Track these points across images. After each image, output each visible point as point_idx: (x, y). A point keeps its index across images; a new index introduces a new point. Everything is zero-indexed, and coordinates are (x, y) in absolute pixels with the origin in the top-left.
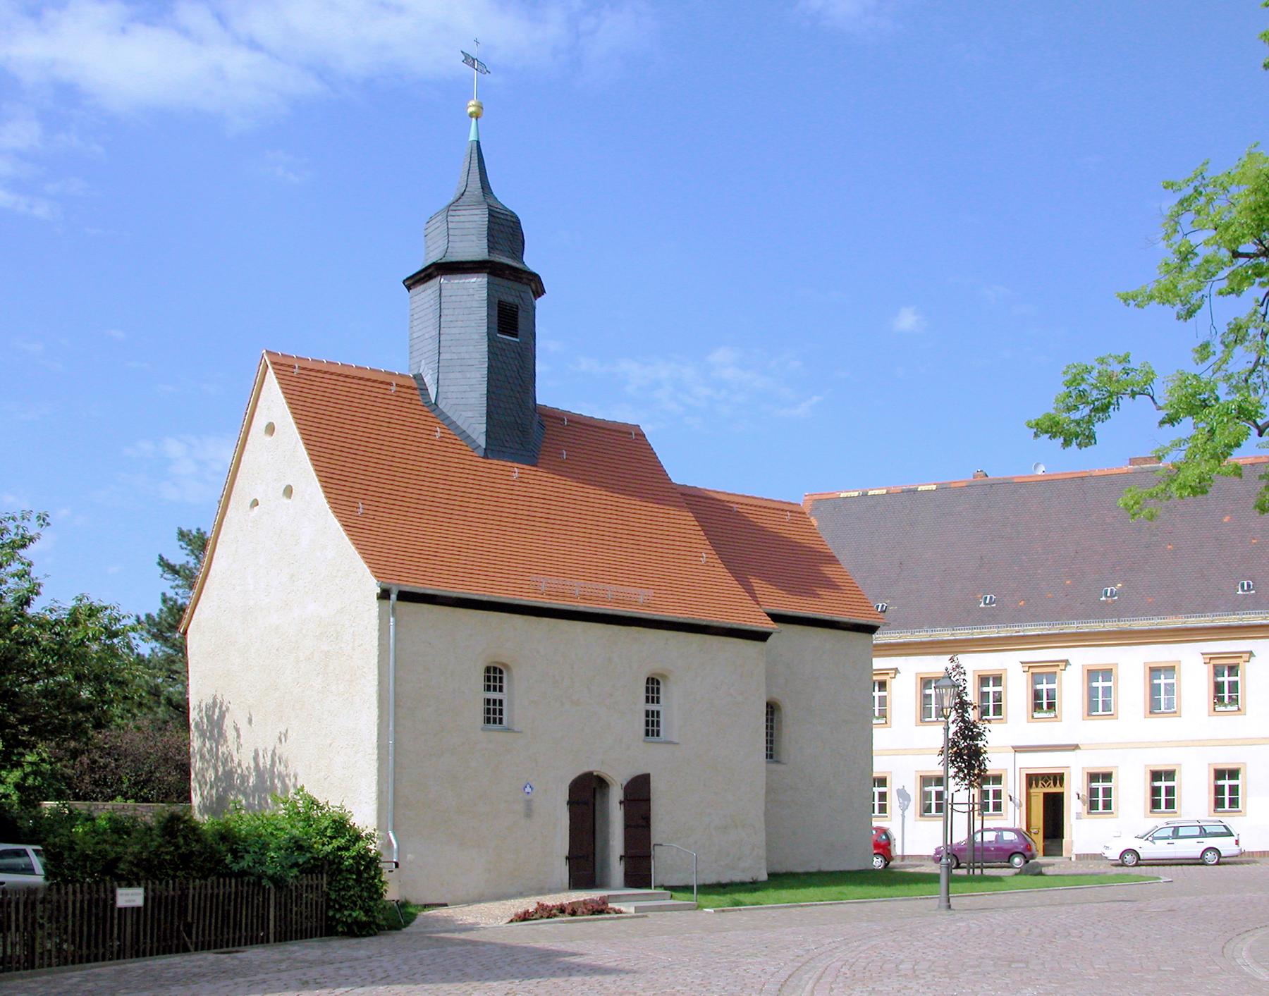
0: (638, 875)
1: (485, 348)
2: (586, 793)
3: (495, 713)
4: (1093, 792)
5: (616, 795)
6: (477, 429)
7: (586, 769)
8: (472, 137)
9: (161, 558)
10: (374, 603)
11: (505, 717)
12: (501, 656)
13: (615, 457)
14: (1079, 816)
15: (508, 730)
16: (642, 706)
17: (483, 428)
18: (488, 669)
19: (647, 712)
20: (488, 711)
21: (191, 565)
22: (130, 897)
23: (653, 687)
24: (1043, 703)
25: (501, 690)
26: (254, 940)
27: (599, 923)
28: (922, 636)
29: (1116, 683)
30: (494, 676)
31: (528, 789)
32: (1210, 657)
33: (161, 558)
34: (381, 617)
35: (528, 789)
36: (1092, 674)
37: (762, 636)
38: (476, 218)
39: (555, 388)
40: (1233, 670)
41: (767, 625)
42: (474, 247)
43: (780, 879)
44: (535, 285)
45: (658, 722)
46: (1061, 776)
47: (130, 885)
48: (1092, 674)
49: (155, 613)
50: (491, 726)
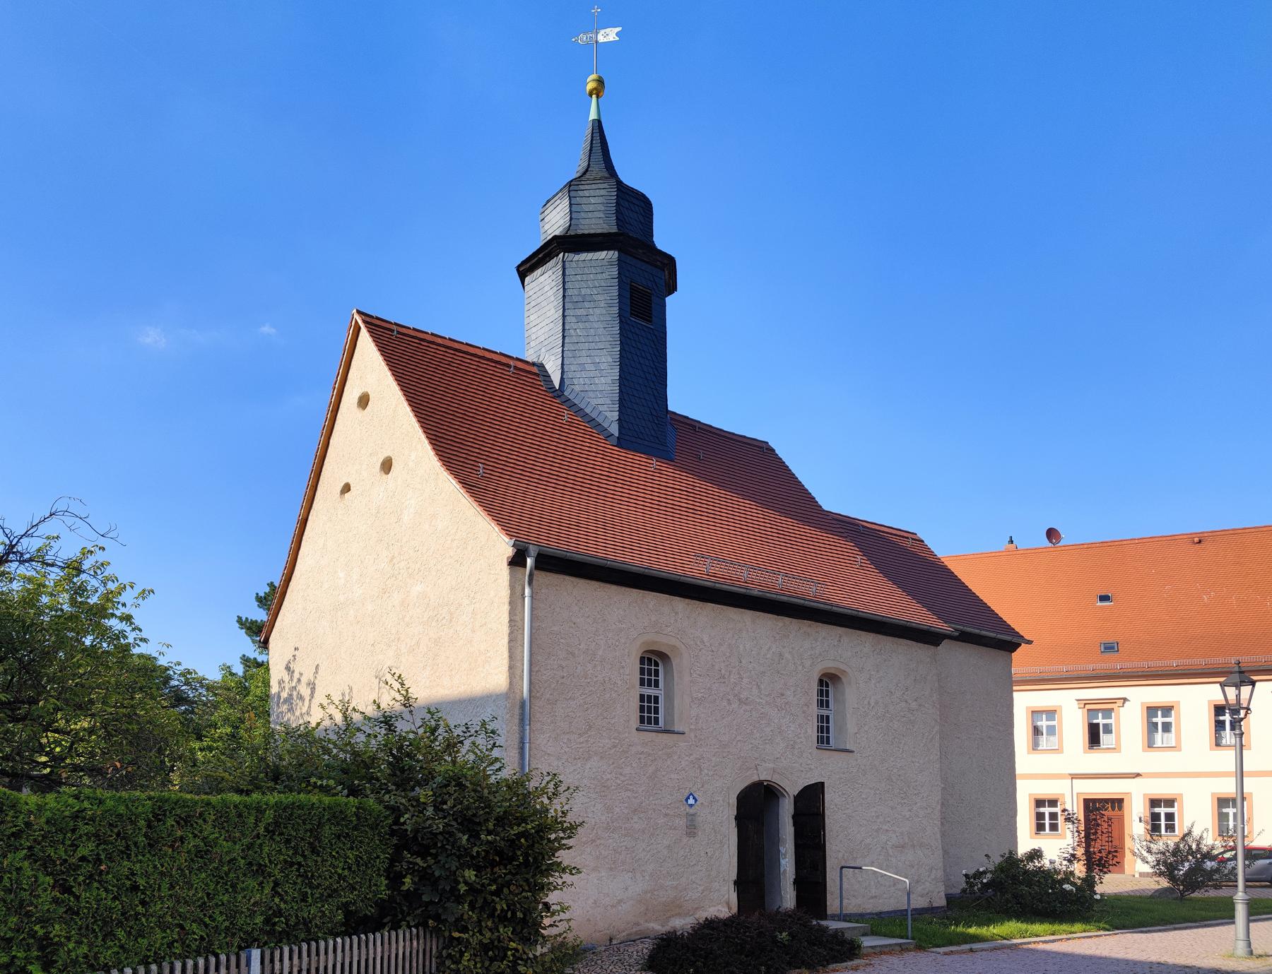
1: (616, 330)
2: (756, 804)
3: (649, 712)
4: (1155, 817)
5: (786, 810)
6: (610, 417)
7: (755, 778)
8: (593, 115)
9: (239, 620)
10: (504, 571)
11: (661, 716)
12: (663, 641)
13: (748, 468)
16: (814, 710)
17: (616, 415)
20: (642, 709)
23: (828, 682)
25: (657, 685)
30: (653, 663)
31: (691, 801)
32: (1085, 703)
33: (239, 620)
34: (512, 587)
35: (691, 801)
38: (603, 192)
39: (687, 395)
42: (598, 220)
44: (667, 264)
45: (828, 728)
46: (1121, 801)
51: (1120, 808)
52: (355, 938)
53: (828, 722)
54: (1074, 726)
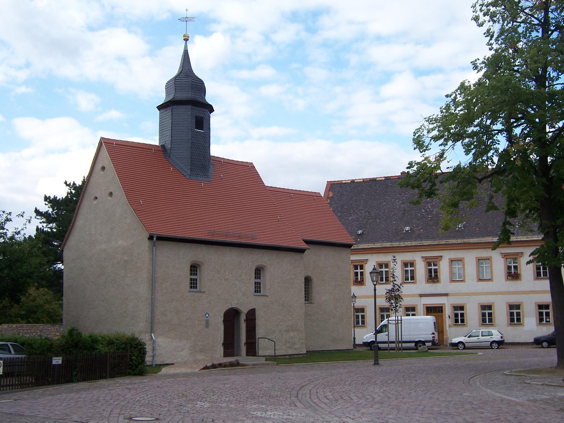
0: (252, 349)
2: (231, 316)
5: (243, 317)
9: (36, 209)
10: (147, 243)
14: (450, 326)
15: (200, 292)
16: (253, 280)
18: (191, 266)
19: (255, 283)
21: (50, 212)
22: (57, 361)
23: (258, 272)
24: (433, 277)
25: (196, 275)
26: (105, 377)
27: (236, 370)
28: (378, 245)
29: (439, 267)
31: (207, 315)
32: (425, 258)
33: (36, 209)
36: (406, 264)
37: (302, 251)
40: (362, 267)
41: (304, 246)
43: (313, 356)
47: (57, 356)
48: (406, 264)
49: (33, 236)
50: (193, 290)
51: (442, 311)
52: (8, 379)
53: (260, 284)
54: (421, 270)
